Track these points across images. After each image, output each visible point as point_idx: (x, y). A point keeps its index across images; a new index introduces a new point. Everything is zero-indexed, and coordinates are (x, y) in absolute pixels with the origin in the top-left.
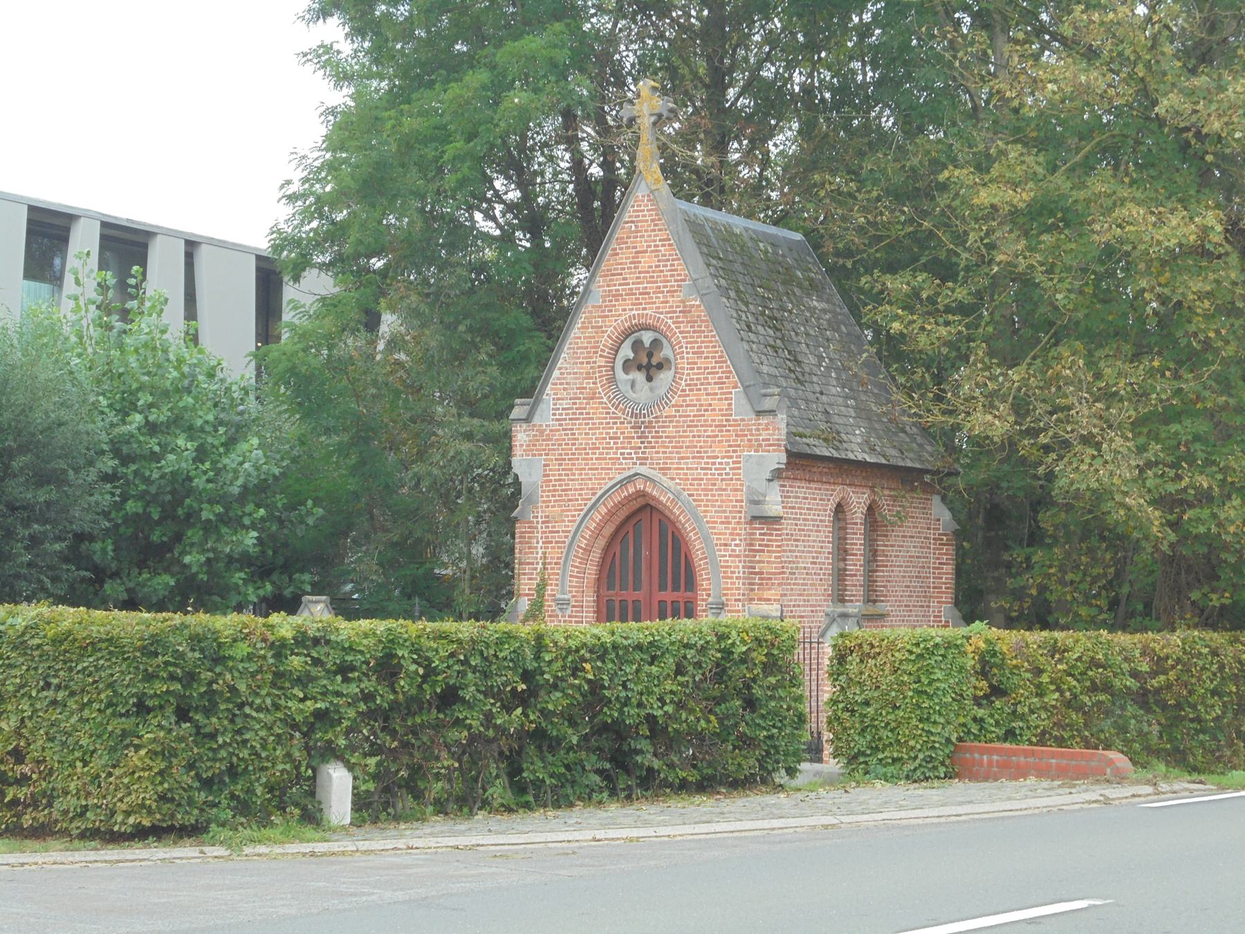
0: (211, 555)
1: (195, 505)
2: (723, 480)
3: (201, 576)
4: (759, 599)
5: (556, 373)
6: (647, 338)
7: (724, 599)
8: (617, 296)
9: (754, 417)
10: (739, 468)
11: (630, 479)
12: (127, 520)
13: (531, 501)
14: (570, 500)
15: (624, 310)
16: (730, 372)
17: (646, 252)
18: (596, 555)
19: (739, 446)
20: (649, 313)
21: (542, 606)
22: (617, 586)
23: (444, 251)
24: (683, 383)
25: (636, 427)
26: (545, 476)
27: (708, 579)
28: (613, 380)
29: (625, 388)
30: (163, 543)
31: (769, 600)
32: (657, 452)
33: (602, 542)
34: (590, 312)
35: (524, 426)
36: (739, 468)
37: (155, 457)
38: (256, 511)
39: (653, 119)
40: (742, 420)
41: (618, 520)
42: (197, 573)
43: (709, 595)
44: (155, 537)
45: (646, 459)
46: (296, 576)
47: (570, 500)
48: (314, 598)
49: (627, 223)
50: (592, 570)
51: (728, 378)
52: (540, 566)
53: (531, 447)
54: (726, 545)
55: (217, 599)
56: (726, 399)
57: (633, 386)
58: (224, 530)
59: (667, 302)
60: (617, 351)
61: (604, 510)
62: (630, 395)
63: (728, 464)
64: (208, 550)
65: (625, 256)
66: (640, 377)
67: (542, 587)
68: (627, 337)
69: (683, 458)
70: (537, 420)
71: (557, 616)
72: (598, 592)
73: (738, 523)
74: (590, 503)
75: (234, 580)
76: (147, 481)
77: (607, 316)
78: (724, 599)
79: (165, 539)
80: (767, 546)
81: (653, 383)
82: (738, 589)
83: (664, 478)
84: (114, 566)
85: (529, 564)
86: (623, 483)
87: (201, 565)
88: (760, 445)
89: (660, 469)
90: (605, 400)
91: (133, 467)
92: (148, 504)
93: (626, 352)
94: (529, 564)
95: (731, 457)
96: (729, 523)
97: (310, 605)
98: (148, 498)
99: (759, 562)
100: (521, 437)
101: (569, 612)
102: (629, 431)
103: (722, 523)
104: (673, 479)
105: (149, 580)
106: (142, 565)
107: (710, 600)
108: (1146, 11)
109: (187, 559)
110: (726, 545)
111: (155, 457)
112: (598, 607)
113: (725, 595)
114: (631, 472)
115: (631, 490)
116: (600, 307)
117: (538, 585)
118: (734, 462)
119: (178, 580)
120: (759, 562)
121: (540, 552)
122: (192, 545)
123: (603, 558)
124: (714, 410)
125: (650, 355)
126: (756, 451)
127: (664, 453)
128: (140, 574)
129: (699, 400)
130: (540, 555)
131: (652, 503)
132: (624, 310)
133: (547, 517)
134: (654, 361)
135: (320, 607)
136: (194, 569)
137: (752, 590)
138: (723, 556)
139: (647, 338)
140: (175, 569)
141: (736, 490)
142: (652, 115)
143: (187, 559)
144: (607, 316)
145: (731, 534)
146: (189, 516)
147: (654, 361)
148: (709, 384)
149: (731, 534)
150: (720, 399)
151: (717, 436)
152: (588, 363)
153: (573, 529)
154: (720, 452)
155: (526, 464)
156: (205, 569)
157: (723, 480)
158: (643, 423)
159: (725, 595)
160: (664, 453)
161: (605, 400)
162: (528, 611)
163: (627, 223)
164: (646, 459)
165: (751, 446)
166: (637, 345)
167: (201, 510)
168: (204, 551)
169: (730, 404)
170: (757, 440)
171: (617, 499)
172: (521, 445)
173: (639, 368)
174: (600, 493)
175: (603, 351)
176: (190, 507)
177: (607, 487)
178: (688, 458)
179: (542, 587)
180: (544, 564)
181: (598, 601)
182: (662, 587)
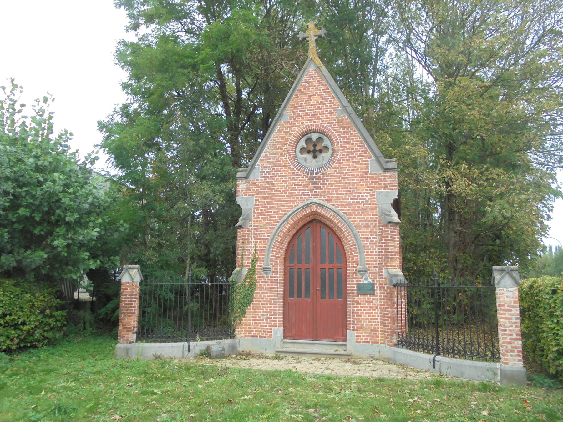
0: (70, 241)
1: (62, 214)
2: (364, 204)
3: (63, 253)
4: (392, 266)
5: (263, 155)
6: (314, 137)
7: (367, 266)
8: (298, 116)
9: (382, 172)
10: (374, 198)
11: (308, 205)
12: (20, 220)
13: (248, 217)
14: (270, 217)
15: (303, 123)
16: (367, 151)
17: (315, 95)
18: (285, 245)
19: (374, 187)
20: (317, 124)
21: (254, 272)
22: (296, 261)
23: (209, 92)
24: (339, 157)
25: (311, 179)
26: (256, 205)
27: (357, 256)
28: (295, 157)
29: (302, 161)
30: (41, 235)
31: (395, 266)
32: (325, 192)
33: (288, 239)
34: (283, 125)
35: (244, 181)
36: (374, 198)
37: (40, 184)
38: (96, 219)
39: (316, 38)
40: (375, 174)
41: (298, 227)
42: (61, 252)
43: (357, 264)
44: (37, 231)
45: (318, 195)
46: (112, 258)
47: (270, 217)
48: (131, 266)
49: (303, 83)
50: (282, 253)
51: (366, 153)
52: (253, 251)
53: (247, 192)
54: (367, 238)
55: (70, 268)
56: (365, 164)
57: (305, 160)
58: (78, 229)
59: (328, 118)
60: (297, 143)
61: (292, 222)
62: (305, 164)
63: (367, 196)
64: (68, 239)
65: (302, 98)
66: (309, 157)
67: (254, 262)
68: (304, 136)
69: (339, 194)
70: (251, 178)
71: (263, 277)
72: (284, 264)
73: (375, 226)
74: (283, 219)
75: (83, 256)
76: (34, 197)
77: (293, 126)
78: (367, 266)
79: (42, 233)
80: (394, 238)
81: (317, 159)
82: (376, 261)
83: (328, 204)
84: (9, 246)
85: (248, 250)
86: (303, 208)
87: (64, 247)
88: (387, 186)
89: (326, 200)
90: (292, 166)
91: (25, 189)
92: (33, 211)
93: (302, 144)
94: (248, 250)
95: (369, 193)
96: (369, 226)
97: (130, 270)
98: (34, 208)
99: (391, 246)
100: (242, 186)
101: (270, 275)
102: (306, 181)
103: (365, 227)
104: (333, 205)
105: (31, 254)
106: (27, 248)
107: (358, 267)
108: (157, 228)
109: (56, 243)
110: (367, 238)
111: (40, 183)
112: (285, 272)
113: (367, 264)
114: (310, 202)
115: (308, 211)
116: (289, 122)
117: (252, 261)
118: (371, 195)
119: (49, 256)
120: (391, 246)
121: (253, 244)
122: (58, 236)
123: (288, 248)
124: (358, 169)
125: (315, 146)
126: (384, 189)
127: (328, 192)
128: (25, 252)
129: (349, 165)
130: (253, 245)
131: (319, 218)
132: (303, 123)
133: (257, 226)
134: (318, 148)
135: (135, 271)
136: (59, 249)
137: (388, 261)
138: (365, 244)
139: (314, 137)
140: (48, 250)
141: (373, 209)
142: (315, 36)
143: (56, 243)
144: (293, 126)
145: (370, 232)
146: (57, 221)
147: (318, 148)
148: (354, 157)
149: (370, 232)
150: (361, 164)
151: (360, 182)
152: (281, 149)
153: (273, 233)
154: (362, 190)
155: (243, 200)
156: (66, 249)
157: (364, 204)
158: (315, 178)
159: (367, 264)
160: (328, 192)
161: (292, 166)
162: (247, 274)
163: (303, 83)
164: (318, 195)
165: (381, 187)
166: (308, 140)
167: (65, 216)
168: (65, 239)
169: (368, 166)
170: (384, 184)
171: (300, 216)
172: (242, 191)
173: (309, 152)
174: (289, 213)
175: (290, 143)
176: (59, 216)
177: (294, 210)
178: (343, 194)
179: (254, 262)
180: (255, 250)
181: (284, 269)
182: (322, 261)
